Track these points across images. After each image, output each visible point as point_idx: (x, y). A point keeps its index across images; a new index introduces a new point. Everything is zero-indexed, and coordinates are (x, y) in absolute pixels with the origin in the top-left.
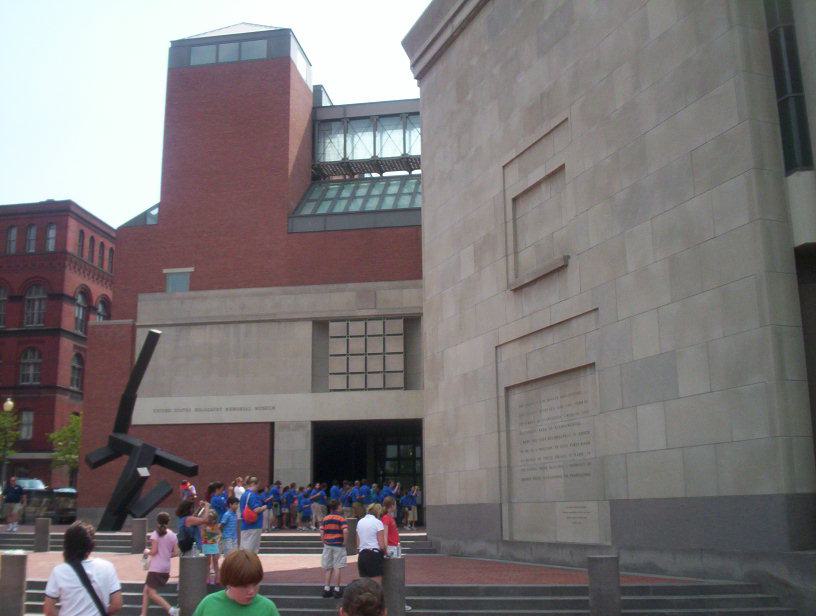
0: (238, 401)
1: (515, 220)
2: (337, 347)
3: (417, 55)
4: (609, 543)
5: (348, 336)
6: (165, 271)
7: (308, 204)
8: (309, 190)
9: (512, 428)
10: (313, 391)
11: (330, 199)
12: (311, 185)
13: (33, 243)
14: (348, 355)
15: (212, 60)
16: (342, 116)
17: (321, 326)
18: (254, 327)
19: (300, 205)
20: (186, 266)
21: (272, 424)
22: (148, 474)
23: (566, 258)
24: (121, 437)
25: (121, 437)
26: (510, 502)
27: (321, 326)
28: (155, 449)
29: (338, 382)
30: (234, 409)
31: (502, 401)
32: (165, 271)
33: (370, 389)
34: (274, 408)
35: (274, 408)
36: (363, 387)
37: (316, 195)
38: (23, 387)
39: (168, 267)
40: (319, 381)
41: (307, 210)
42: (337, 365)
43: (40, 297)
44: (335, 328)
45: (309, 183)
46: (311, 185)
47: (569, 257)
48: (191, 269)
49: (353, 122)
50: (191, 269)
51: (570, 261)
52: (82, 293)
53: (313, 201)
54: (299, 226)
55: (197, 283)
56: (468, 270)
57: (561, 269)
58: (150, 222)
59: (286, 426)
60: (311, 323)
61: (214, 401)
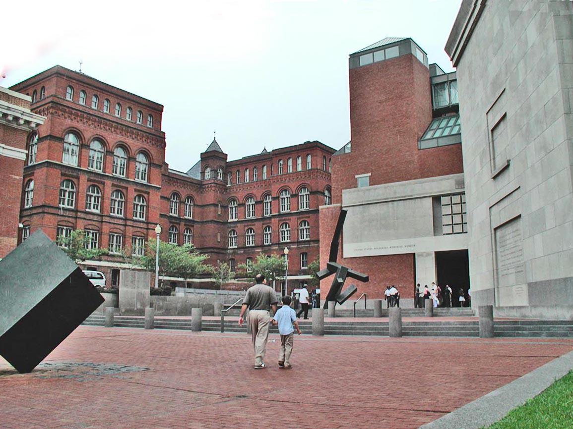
0: (395, 243)
1: (493, 141)
2: (446, 210)
3: (452, 55)
4: (528, 305)
5: (451, 204)
6: (356, 176)
7: (429, 132)
8: (431, 124)
9: (498, 249)
10: (434, 236)
11: (450, 127)
12: (433, 120)
13: (310, 164)
14: (452, 214)
15: (371, 61)
16: (446, 80)
17: (437, 199)
18: (419, 199)
19: (425, 133)
20: (367, 173)
21: (414, 254)
22: (397, 292)
23: (509, 161)
24: (333, 264)
25: (333, 264)
26: (498, 288)
27: (437, 199)
28: (347, 269)
29: (448, 230)
30: (394, 247)
31: (493, 235)
32: (356, 176)
33: (455, 234)
34: (414, 245)
35: (414, 245)
36: (452, 232)
37: (435, 126)
38: (302, 241)
39: (358, 174)
40: (437, 228)
41: (429, 136)
42: (446, 220)
43: (287, 196)
44: (444, 200)
45: (431, 120)
46: (433, 120)
47: (510, 160)
48: (370, 174)
49: (453, 83)
50: (370, 174)
51: (510, 162)
52: (327, 189)
53: (432, 130)
54: (424, 145)
55: (373, 182)
56: (478, 169)
57: (507, 167)
58: (348, 151)
59: (421, 255)
60: (431, 198)
61: (363, 245)
